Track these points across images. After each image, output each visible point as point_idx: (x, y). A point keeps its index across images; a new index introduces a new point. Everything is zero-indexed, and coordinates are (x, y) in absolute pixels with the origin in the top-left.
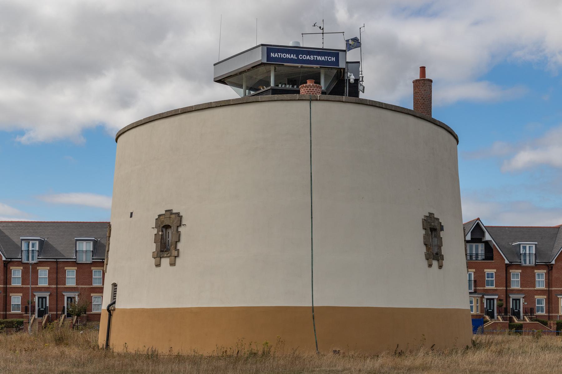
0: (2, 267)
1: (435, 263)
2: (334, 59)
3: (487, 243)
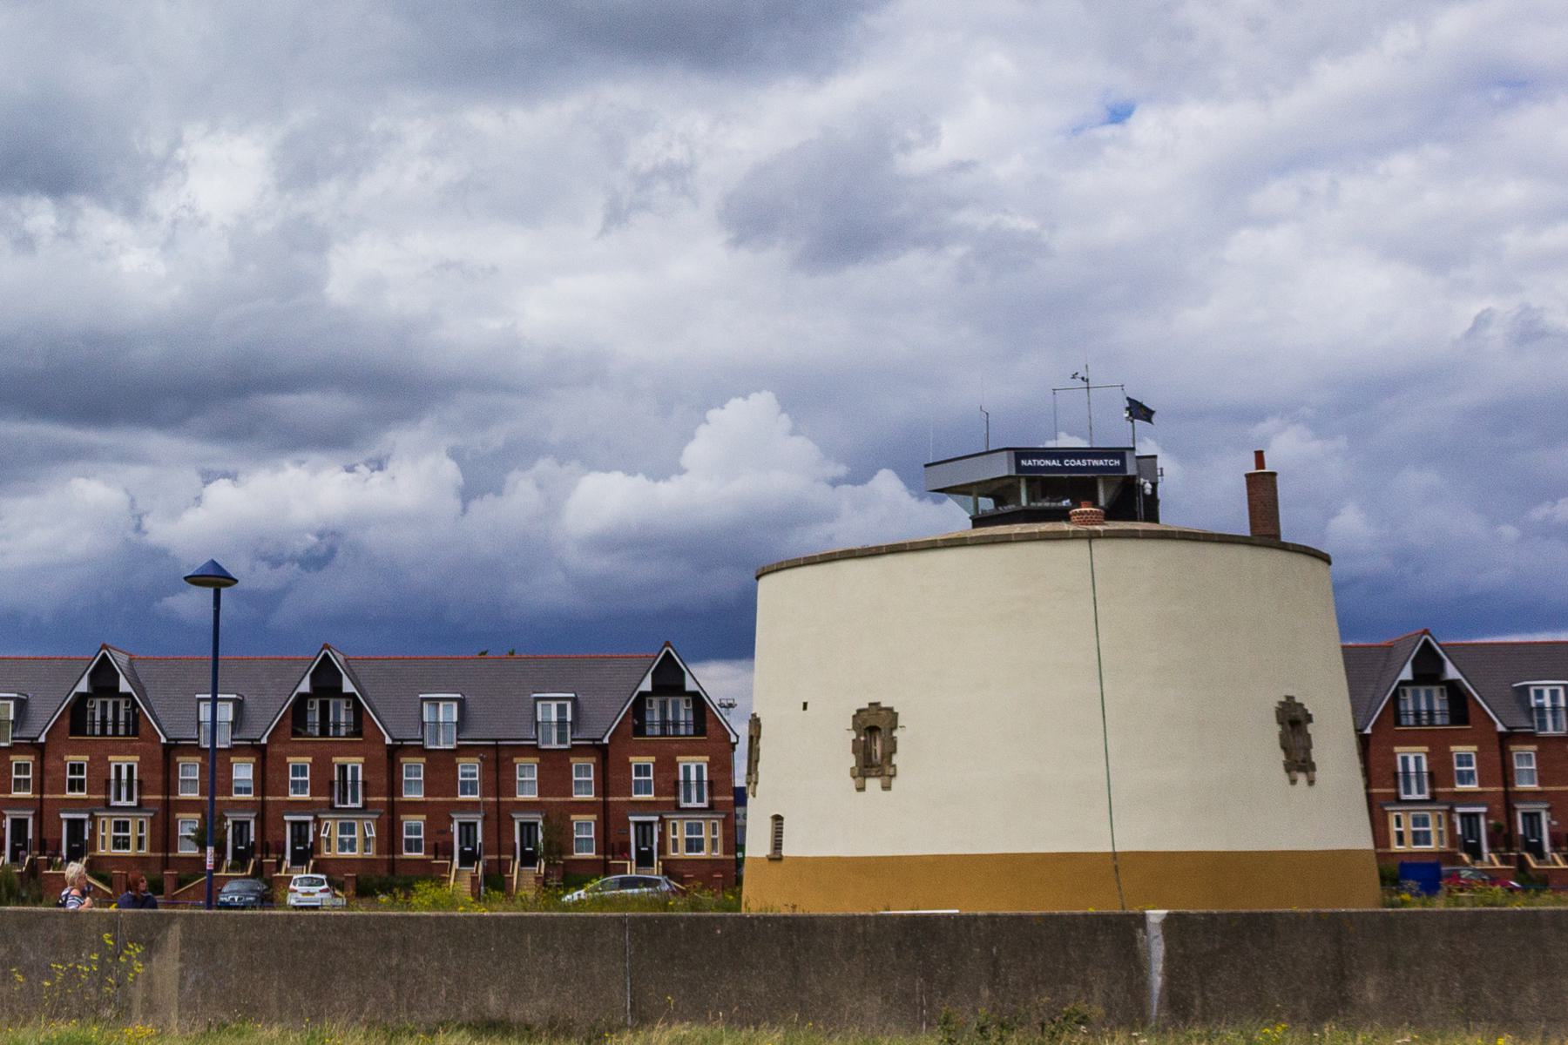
0: (385, 758)
1: (1302, 778)
2: (1117, 462)
3: (1453, 686)
